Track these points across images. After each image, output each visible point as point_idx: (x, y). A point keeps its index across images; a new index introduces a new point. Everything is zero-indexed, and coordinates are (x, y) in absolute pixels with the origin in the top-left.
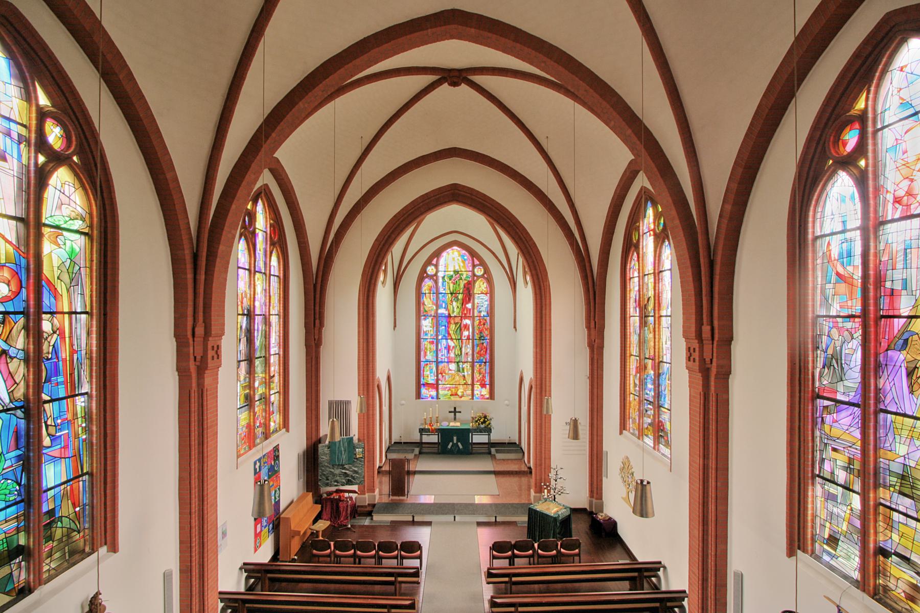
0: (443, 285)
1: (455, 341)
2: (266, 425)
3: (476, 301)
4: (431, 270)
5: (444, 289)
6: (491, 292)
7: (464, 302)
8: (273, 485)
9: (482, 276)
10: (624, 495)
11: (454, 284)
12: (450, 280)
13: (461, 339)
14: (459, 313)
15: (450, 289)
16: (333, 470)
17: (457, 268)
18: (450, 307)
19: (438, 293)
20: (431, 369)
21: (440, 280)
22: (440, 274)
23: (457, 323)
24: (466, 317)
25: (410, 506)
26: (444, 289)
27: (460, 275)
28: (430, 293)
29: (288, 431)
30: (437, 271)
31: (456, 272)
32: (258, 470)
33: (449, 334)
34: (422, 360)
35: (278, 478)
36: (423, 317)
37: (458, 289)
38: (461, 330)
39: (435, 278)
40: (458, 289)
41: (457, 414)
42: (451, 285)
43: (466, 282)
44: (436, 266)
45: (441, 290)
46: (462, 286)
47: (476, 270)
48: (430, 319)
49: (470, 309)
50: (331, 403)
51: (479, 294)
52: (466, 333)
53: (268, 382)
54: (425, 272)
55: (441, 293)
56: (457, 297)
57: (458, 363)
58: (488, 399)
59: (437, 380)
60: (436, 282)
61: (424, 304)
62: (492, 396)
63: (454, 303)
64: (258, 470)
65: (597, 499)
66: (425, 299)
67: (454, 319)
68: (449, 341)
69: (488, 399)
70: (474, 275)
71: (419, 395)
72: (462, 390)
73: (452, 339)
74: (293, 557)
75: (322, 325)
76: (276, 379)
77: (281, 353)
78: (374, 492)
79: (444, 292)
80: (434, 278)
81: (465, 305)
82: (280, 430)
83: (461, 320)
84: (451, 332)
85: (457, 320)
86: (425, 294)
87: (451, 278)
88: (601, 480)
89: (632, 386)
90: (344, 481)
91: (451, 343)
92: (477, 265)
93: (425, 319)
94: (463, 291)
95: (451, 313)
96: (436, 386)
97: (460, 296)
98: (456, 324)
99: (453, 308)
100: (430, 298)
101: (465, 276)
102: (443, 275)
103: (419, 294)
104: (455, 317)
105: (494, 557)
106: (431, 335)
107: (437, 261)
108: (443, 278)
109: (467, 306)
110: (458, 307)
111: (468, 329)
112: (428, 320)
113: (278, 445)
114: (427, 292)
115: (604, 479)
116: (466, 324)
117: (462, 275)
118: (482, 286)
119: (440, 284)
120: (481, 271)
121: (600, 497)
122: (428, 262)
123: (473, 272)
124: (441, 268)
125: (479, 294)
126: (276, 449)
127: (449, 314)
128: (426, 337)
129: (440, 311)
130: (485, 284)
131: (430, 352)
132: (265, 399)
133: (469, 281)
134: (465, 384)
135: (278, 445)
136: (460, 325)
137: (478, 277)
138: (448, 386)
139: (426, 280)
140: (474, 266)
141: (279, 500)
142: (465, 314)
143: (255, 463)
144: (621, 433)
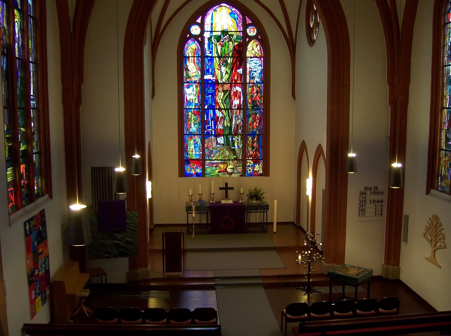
0: (209, 47)
1: (223, 111)
2: (30, 186)
3: (248, 66)
4: (195, 30)
5: (211, 52)
6: (266, 57)
7: (234, 67)
8: (42, 252)
9: (255, 38)
10: (429, 254)
11: (222, 46)
12: (218, 41)
13: (231, 109)
14: (228, 79)
15: (217, 52)
16: (103, 241)
17: (225, 28)
18: (218, 72)
19: (203, 56)
20: (196, 143)
21: (206, 42)
22: (207, 35)
23: (227, 91)
24: (236, 84)
25: (268, 208)
26: (211, 52)
27: (230, 35)
28: (194, 57)
29: (51, 197)
30: (203, 31)
31: (225, 32)
32: (28, 233)
33: (217, 103)
34: (185, 133)
35: (46, 245)
36: (186, 84)
37: (227, 52)
38: (231, 98)
39: (200, 39)
40: (227, 52)
41: (229, 191)
42: (219, 47)
43: (236, 44)
44: (202, 26)
45: (208, 54)
46: (231, 47)
47: (248, 30)
48: (194, 86)
49: (241, 75)
50: (94, 169)
51: (251, 57)
52: (236, 102)
53: (28, 140)
54: (190, 33)
55: (207, 57)
56: (226, 61)
57: (227, 136)
58: (261, 175)
59: (203, 155)
60: (202, 44)
61: (187, 69)
62: (266, 172)
63: (223, 69)
64: (28, 233)
65: (393, 265)
66: (188, 64)
67: (222, 86)
68: (217, 111)
69: (261, 175)
70: (245, 35)
71: (183, 173)
72: (232, 167)
73: (220, 109)
74: (70, 321)
75: (81, 80)
76: (36, 137)
77: (40, 108)
78: (147, 267)
79: (210, 55)
80: (199, 39)
81: (236, 71)
82: (43, 195)
83: (231, 87)
84: (220, 101)
85: (226, 87)
86: (189, 57)
87: (218, 38)
88: (399, 247)
89: (443, 140)
90: (116, 252)
91: (219, 114)
92: (250, 25)
93: (188, 87)
94: (233, 54)
95: (219, 78)
96: (201, 162)
97: (230, 61)
98: (225, 92)
99: (221, 73)
100: (194, 62)
101: (235, 37)
102: (209, 36)
103: (182, 59)
104: (224, 83)
105: (288, 320)
106: (196, 105)
107: (203, 21)
108: (210, 39)
109: (238, 71)
110: (227, 73)
111: (240, 98)
112: (191, 88)
113: (44, 210)
114: (190, 55)
115: (403, 244)
116: (237, 91)
117: (232, 35)
118: (255, 48)
119: (206, 46)
120: (254, 31)
121: (397, 262)
122: (192, 22)
123: (244, 32)
124: (207, 27)
125: (251, 57)
126: (42, 214)
127: (217, 80)
128: (190, 107)
129: (206, 77)
130: (258, 47)
131: (194, 124)
132: (27, 155)
133: (240, 43)
134: (235, 159)
135: (44, 210)
136: (230, 94)
137: (251, 38)
138: (216, 161)
139: (190, 42)
140: (245, 26)
141: (49, 269)
142: (235, 80)
143: (25, 224)
144: (428, 193)
